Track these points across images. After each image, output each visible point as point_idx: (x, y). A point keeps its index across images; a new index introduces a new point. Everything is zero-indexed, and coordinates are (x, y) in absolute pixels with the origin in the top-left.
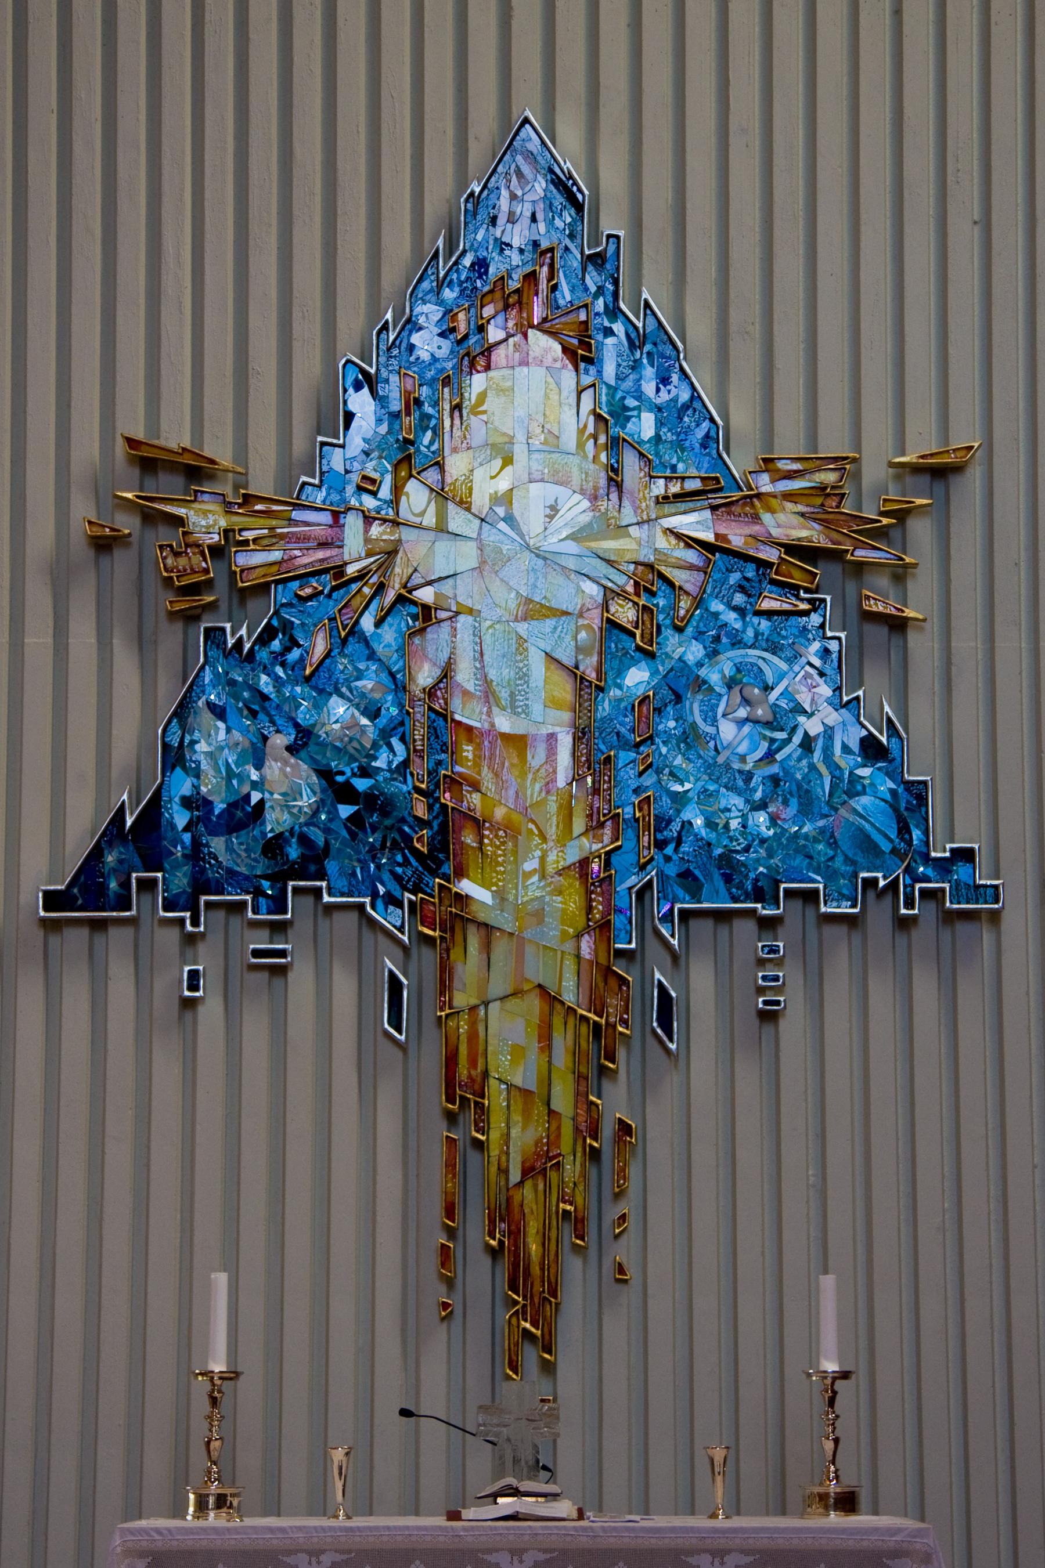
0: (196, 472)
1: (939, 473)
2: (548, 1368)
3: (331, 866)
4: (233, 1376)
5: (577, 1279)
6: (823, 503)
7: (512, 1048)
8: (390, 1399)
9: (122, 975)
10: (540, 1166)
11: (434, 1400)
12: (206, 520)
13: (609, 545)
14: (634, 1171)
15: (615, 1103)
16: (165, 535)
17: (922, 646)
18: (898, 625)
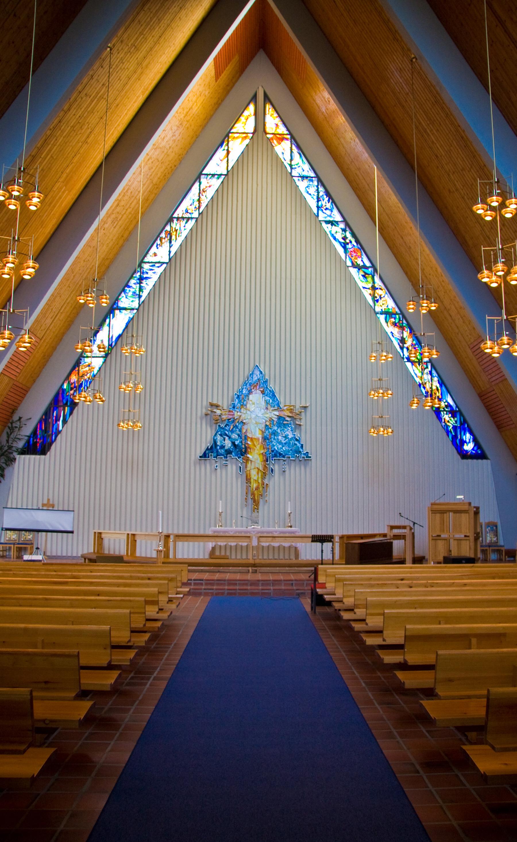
0: (217, 406)
1: (305, 408)
2: (258, 512)
3: (233, 453)
4: (222, 512)
5: (261, 502)
6: (291, 411)
7: (254, 475)
9: (212, 463)
10: (257, 488)
12: (218, 412)
13: (266, 415)
14: (268, 489)
15: (266, 481)
16: (213, 414)
17: (303, 428)
18: (300, 425)
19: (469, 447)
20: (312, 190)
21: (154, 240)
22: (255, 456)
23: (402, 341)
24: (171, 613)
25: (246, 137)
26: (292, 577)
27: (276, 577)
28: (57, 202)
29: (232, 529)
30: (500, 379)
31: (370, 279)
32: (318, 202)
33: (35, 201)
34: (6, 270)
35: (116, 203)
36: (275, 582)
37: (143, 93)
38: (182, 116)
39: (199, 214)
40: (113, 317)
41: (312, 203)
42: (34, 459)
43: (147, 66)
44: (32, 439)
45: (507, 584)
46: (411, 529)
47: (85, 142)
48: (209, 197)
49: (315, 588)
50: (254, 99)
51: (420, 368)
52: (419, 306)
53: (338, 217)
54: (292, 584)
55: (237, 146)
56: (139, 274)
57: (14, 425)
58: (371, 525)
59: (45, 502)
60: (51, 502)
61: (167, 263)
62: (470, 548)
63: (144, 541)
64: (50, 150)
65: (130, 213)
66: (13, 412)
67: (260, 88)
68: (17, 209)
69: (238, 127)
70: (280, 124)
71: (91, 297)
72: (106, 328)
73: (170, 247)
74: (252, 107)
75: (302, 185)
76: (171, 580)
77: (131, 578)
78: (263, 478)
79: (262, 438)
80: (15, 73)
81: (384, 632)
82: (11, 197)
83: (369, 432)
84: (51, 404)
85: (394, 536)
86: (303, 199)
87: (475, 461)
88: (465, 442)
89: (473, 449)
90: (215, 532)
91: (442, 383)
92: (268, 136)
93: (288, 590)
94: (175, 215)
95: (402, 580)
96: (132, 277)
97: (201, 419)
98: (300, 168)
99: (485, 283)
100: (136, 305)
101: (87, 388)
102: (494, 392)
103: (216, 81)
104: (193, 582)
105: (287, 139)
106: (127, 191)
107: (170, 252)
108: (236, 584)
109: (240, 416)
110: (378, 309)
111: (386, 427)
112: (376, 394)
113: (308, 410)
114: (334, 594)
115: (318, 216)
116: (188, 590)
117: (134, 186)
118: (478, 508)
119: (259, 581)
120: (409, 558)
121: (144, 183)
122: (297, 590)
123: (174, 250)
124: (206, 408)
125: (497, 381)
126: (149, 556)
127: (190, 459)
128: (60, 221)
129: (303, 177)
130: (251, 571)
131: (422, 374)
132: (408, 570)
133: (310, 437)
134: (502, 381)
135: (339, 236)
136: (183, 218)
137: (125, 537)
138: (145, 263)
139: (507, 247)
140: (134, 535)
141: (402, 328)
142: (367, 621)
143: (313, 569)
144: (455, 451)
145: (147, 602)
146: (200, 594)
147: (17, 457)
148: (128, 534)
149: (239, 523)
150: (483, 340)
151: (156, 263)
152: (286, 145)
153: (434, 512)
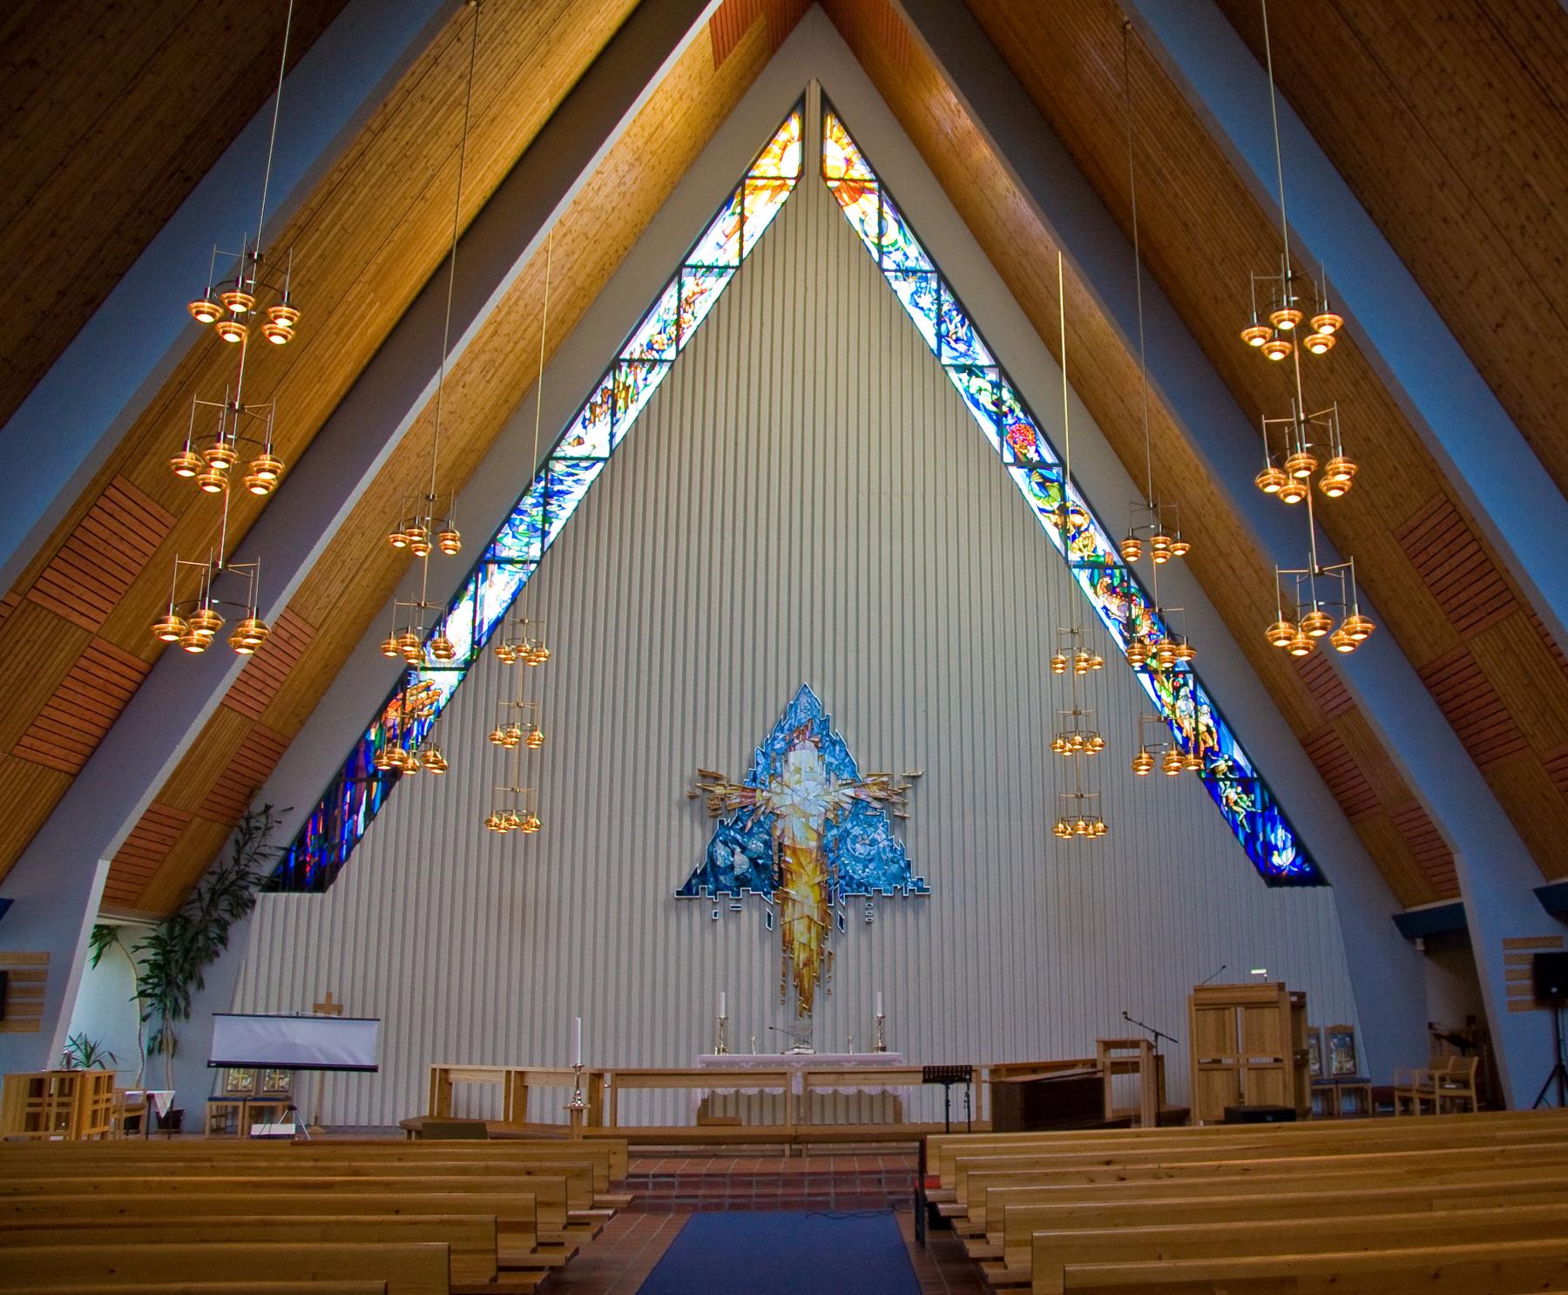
0: (717, 778)
1: (915, 778)
6: (883, 786)
7: (801, 933)
8: (768, 1023)
9: (696, 914)
11: (780, 1024)
12: (719, 790)
13: (828, 798)
15: (828, 946)
18: (904, 818)
19: (1283, 859)
20: (926, 300)
21: (578, 408)
22: (804, 890)
23: (1130, 625)
24: (576, 1251)
25: (781, 187)
26: (881, 1164)
27: (844, 1166)
28: (355, 326)
29: (748, 1056)
30: (1344, 707)
31: (1054, 491)
32: (939, 324)
33: (282, 325)
34: (213, 476)
35: (492, 328)
36: (842, 1177)
37: (551, 93)
38: (640, 143)
39: (678, 353)
40: (484, 580)
41: (927, 328)
42: (287, 900)
43: (560, 39)
44: (293, 855)
45: (1342, 1165)
46: (1150, 1047)
47: (421, 196)
48: (701, 316)
49: (922, 1186)
50: (800, 105)
51: (1169, 685)
52: (1147, 549)
53: (983, 359)
54: (880, 1180)
55: (761, 208)
56: (543, 484)
57: (253, 823)
58: (1058, 1042)
59: (322, 1000)
60: (335, 1001)
61: (605, 460)
62: (1285, 1087)
63: (549, 1089)
64: (340, 215)
65: (524, 350)
66: (251, 795)
67: (814, 82)
68: (241, 343)
69: (766, 166)
70: (856, 158)
71: (420, 535)
72: (465, 606)
73: (613, 425)
74: (794, 125)
75: (904, 289)
76: (580, 1174)
77: (488, 1171)
78: (822, 939)
79: (819, 848)
80: (262, 53)
81: (1034, 1284)
82: (229, 316)
83: (1054, 830)
84: (339, 775)
85: (1113, 1064)
86: (906, 319)
87: (1298, 889)
88: (1276, 847)
89: (1293, 863)
90: (708, 1064)
91: (1218, 717)
92: (831, 184)
93: (870, 1194)
94: (626, 355)
95: (1108, 1163)
96: (526, 492)
97: (681, 808)
98: (900, 254)
99: (1274, 495)
100: (535, 552)
101: (424, 738)
102: (1334, 735)
103: (716, 69)
104: (650, 1180)
105: (871, 191)
106: (516, 303)
107: (612, 435)
108: (750, 1184)
109: (769, 800)
110: (1074, 557)
111: (1091, 820)
112: (1069, 746)
113: (922, 783)
114: (955, 1202)
115: (939, 355)
116: (629, 1198)
117: (532, 290)
118: (1301, 996)
119: (803, 1174)
120: (1148, 1113)
121: (555, 284)
122: (891, 1193)
123: (621, 431)
124: (692, 784)
125: (1338, 711)
126: (548, 1121)
127: (655, 900)
128: (361, 368)
129: (907, 273)
130: (787, 1152)
131: (1176, 698)
132: (1148, 1139)
133: (926, 843)
134: (1346, 712)
135: (986, 399)
136: (642, 361)
137: (502, 1078)
138: (558, 459)
139: (1316, 418)
140: (522, 1074)
141: (1128, 597)
142: (1006, 1259)
143: (917, 1144)
144: (1253, 868)
145: (502, 1227)
146: (665, 1209)
147: (259, 896)
148: (509, 1073)
149: (767, 1044)
150: (1271, 621)
151: (581, 459)
152: (870, 202)
153: (1201, 1006)
